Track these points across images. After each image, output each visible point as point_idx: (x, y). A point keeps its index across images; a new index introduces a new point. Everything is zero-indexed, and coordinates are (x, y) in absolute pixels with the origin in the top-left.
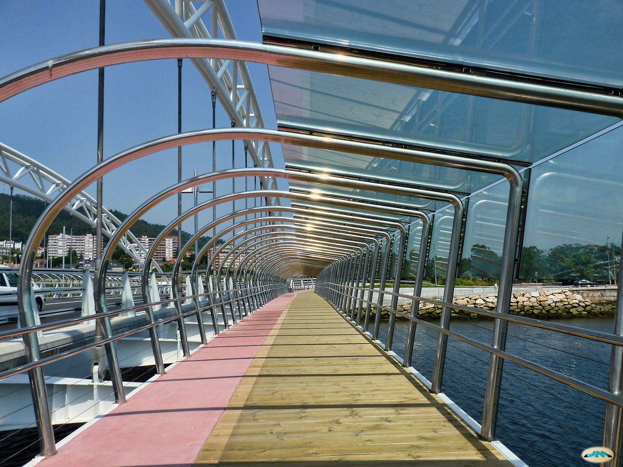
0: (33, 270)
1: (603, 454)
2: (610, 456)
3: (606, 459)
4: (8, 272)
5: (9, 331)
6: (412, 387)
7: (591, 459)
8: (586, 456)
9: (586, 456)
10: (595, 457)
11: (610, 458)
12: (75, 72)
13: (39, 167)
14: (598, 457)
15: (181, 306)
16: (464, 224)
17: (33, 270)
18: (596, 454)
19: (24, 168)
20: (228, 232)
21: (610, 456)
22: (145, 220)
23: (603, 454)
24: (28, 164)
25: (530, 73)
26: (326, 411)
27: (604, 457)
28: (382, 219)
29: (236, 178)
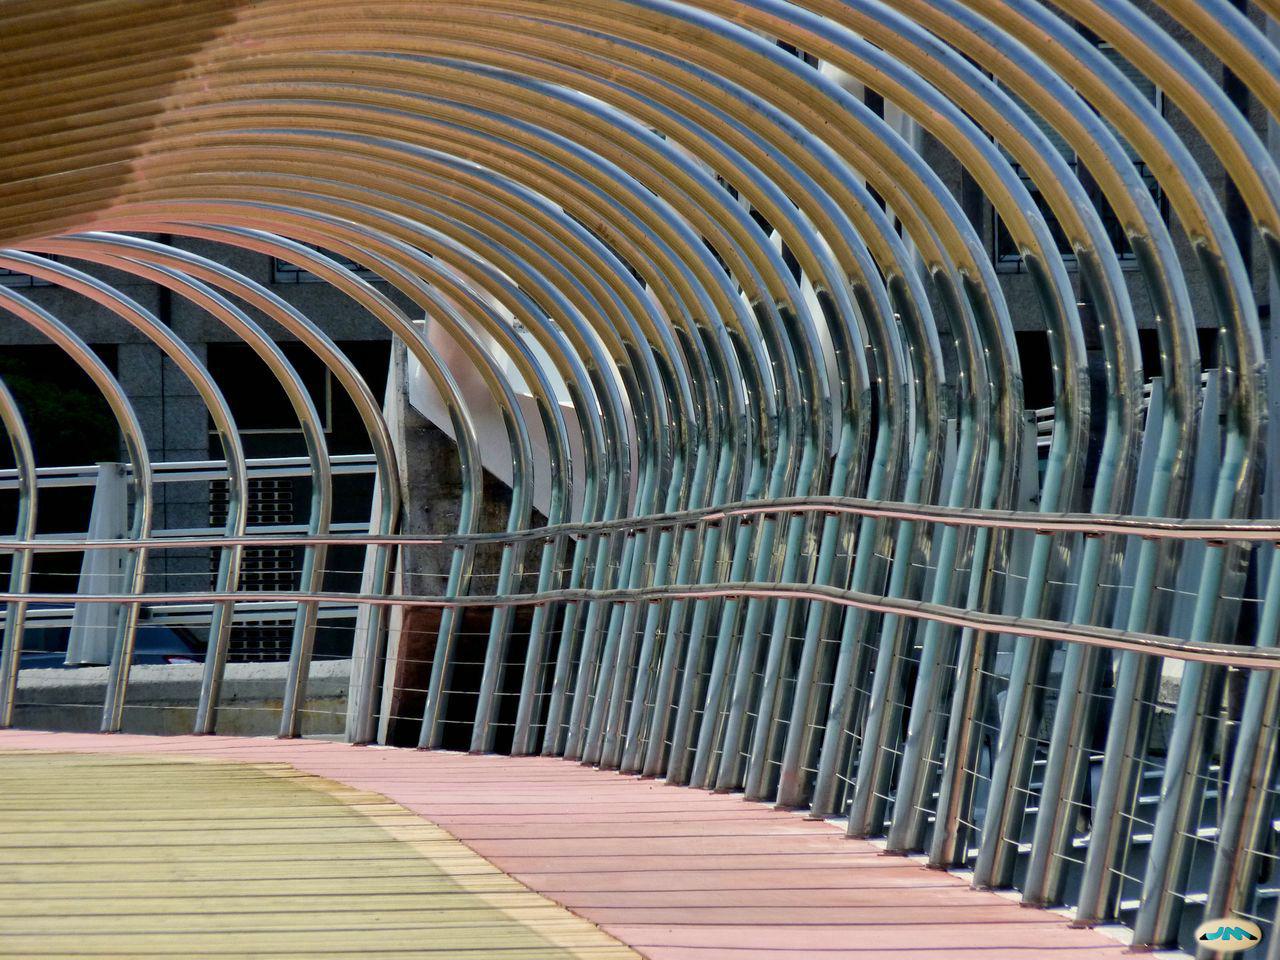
0: (321, 609)
1: (1239, 933)
2: (1252, 938)
3: (1245, 944)
4: (1221, 846)
5: (779, 709)
8: (1204, 938)
9: (1204, 938)
10: (1223, 939)
11: (1254, 942)
12: (734, 833)
14: (1228, 939)
15: (1131, 839)
17: (321, 609)
18: (1225, 934)
19: (963, 862)
20: (87, 241)
21: (1252, 938)
23: (1239, 933)
25: (456, 955)
26: (489, 760)
28: (621, 179)
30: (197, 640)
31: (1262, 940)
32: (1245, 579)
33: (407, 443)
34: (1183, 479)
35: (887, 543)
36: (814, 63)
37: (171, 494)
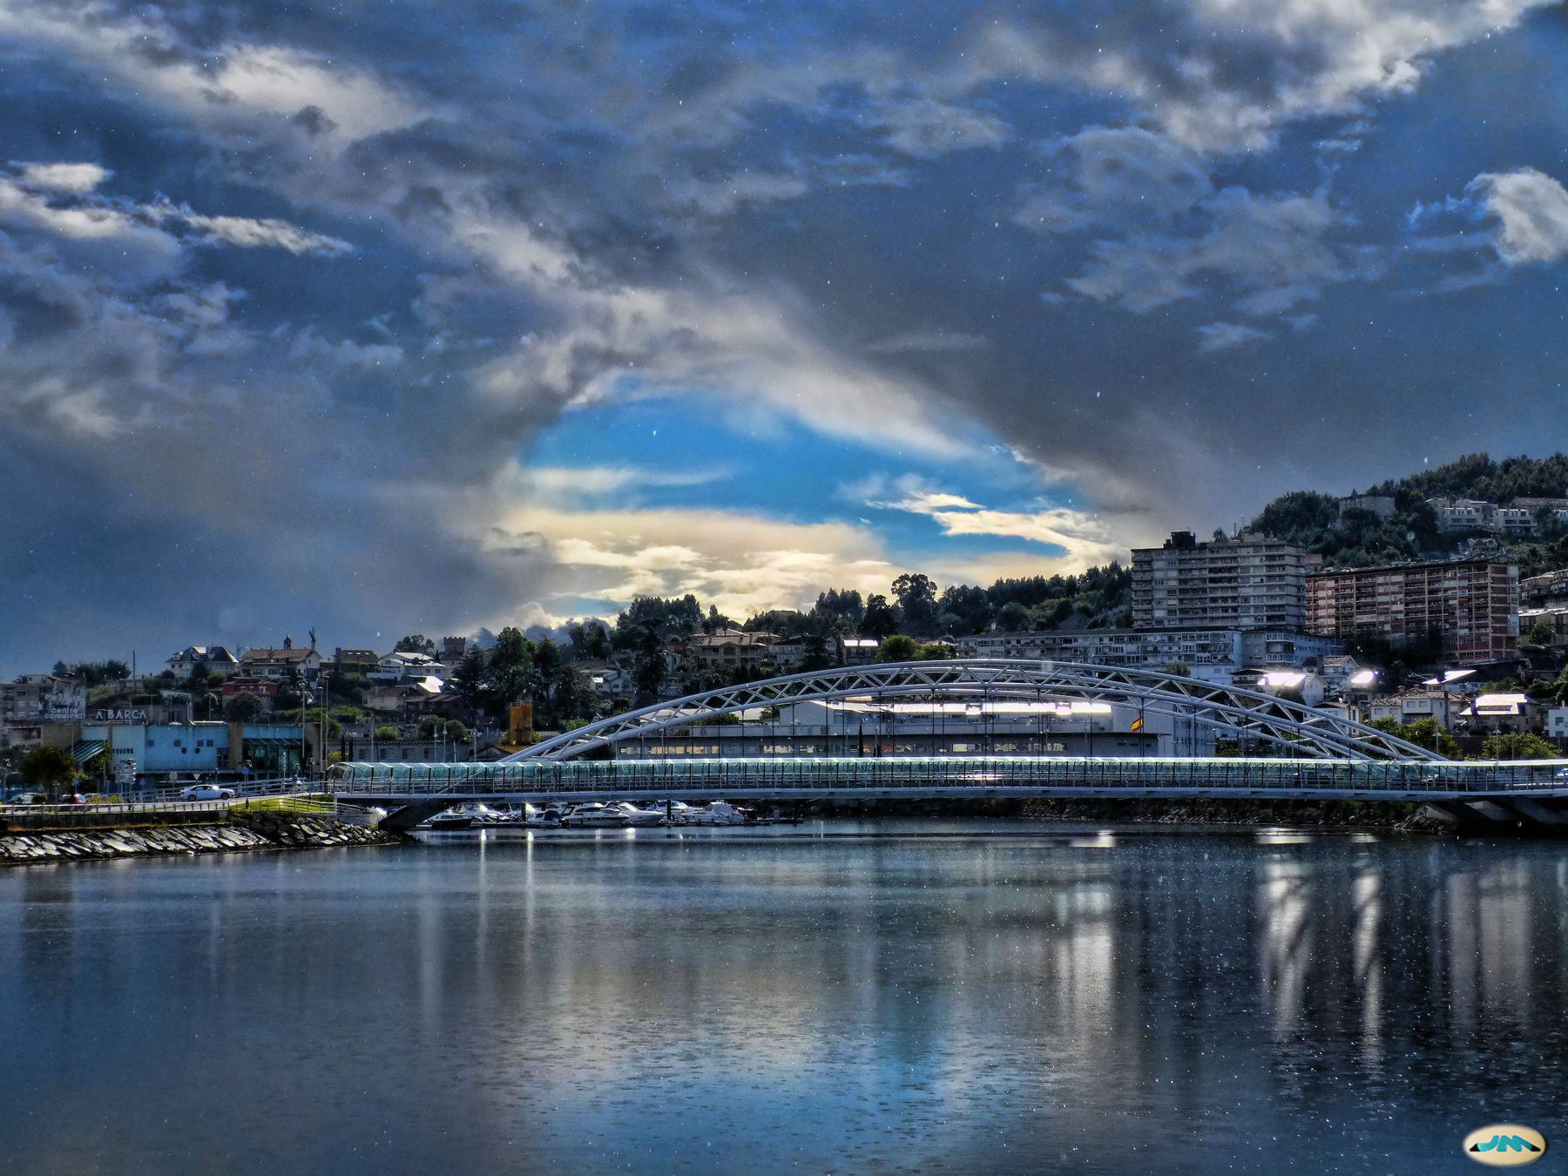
1: (1517, 1143)
2: (1534, 1149)
3: (1526, 1156)
7: (1487, 1157)
8: (1475, 1149)
9: (1475, 1149)
14: (1505, 1150)
18: (1500, 1144)
21: (1534, 1149)
23: (1517, 1143)
27: (1519, 1150)
30: (853, 513)
31: (1545, 1152)
32: (734, 421)
33: (1512, 172)
34: (946, 781)
35: (608, 704)
36: (1186, 673)
37: (419, 749)
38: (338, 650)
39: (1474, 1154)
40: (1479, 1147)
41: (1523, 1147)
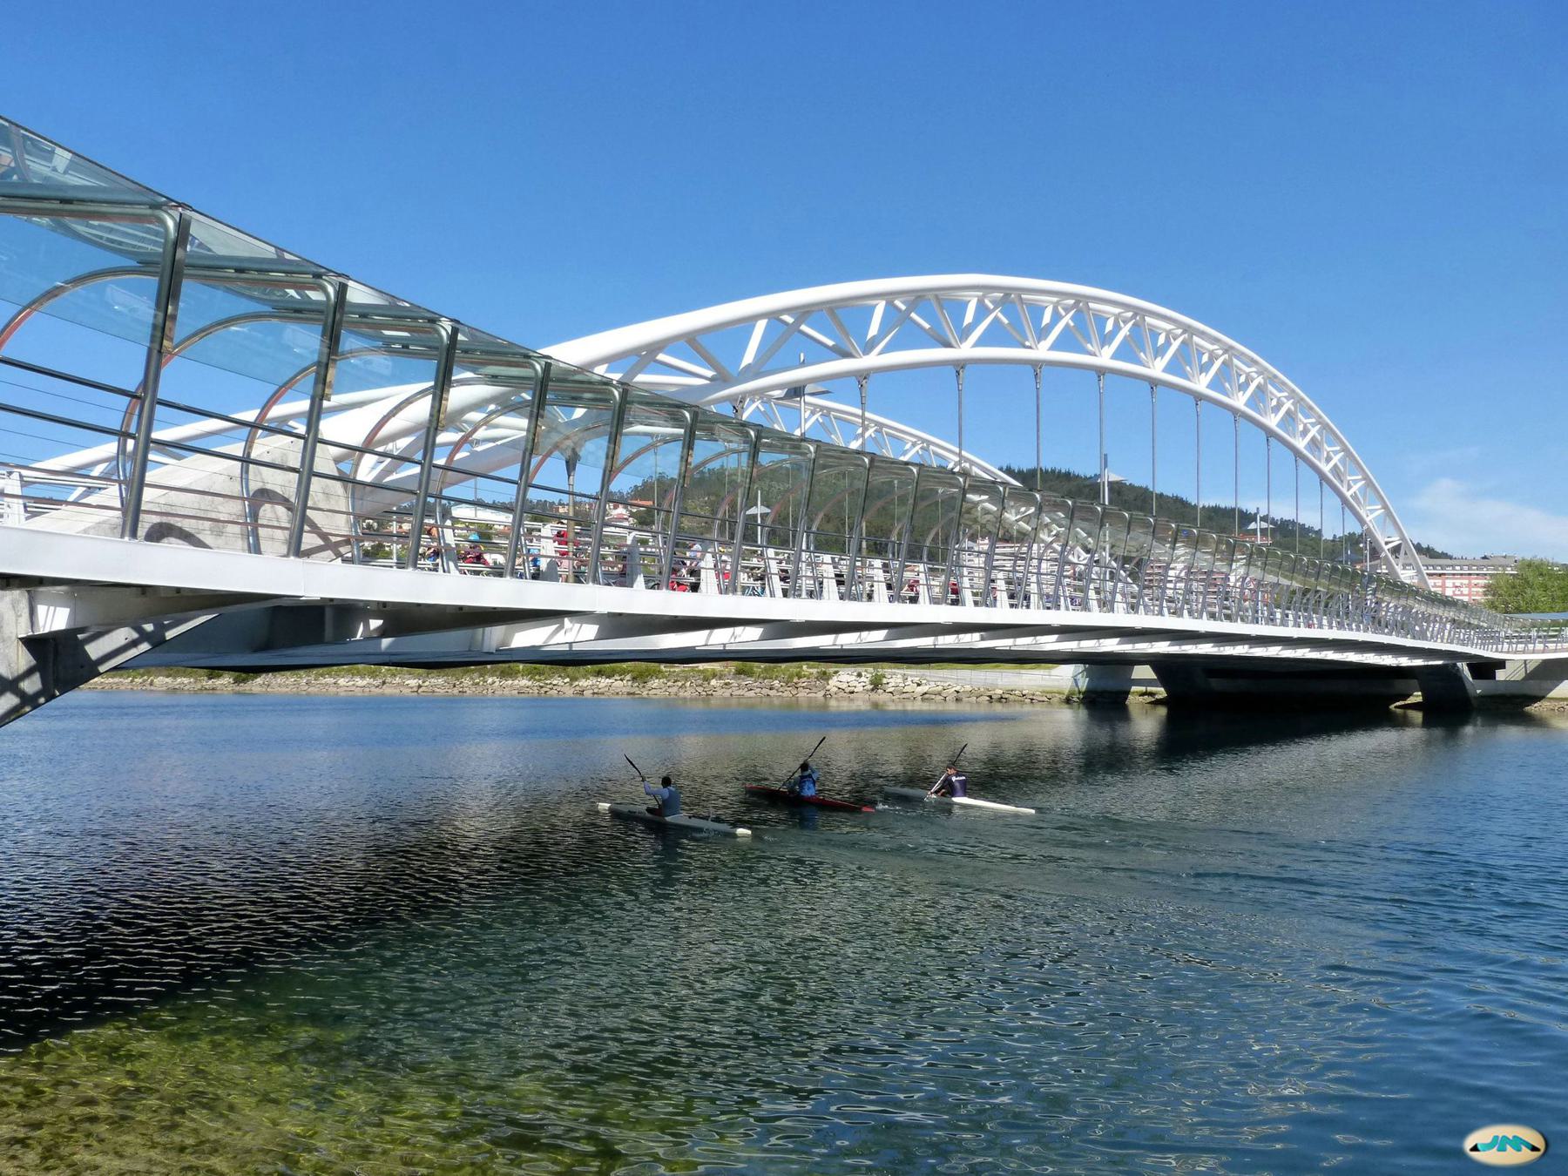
1: (1518, 1143)
2: (1534, 1149)
3: (1526, 1156)
6: (95, 250)
7: (1487, 1157)
8: (1475, 1149)
9: (1475, 1149)
10: (1498, 1150)
13: (929, 443)
14: (1505, 1150)
16: (34, 302)
18: (1500, 1144)
21: (1534, 1149)
22: (256, 488)
23: (1518, 1143)
24: (914, 440)
27: (1519, 1150)
29: (161, 395)
38: (1089, 611)
39: (1474, 1154)
40: (1479, 1147)
41: (1523, 1147)
